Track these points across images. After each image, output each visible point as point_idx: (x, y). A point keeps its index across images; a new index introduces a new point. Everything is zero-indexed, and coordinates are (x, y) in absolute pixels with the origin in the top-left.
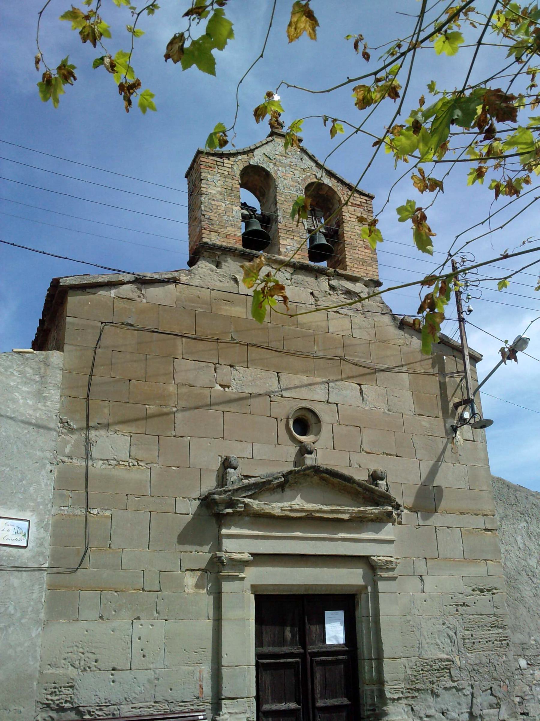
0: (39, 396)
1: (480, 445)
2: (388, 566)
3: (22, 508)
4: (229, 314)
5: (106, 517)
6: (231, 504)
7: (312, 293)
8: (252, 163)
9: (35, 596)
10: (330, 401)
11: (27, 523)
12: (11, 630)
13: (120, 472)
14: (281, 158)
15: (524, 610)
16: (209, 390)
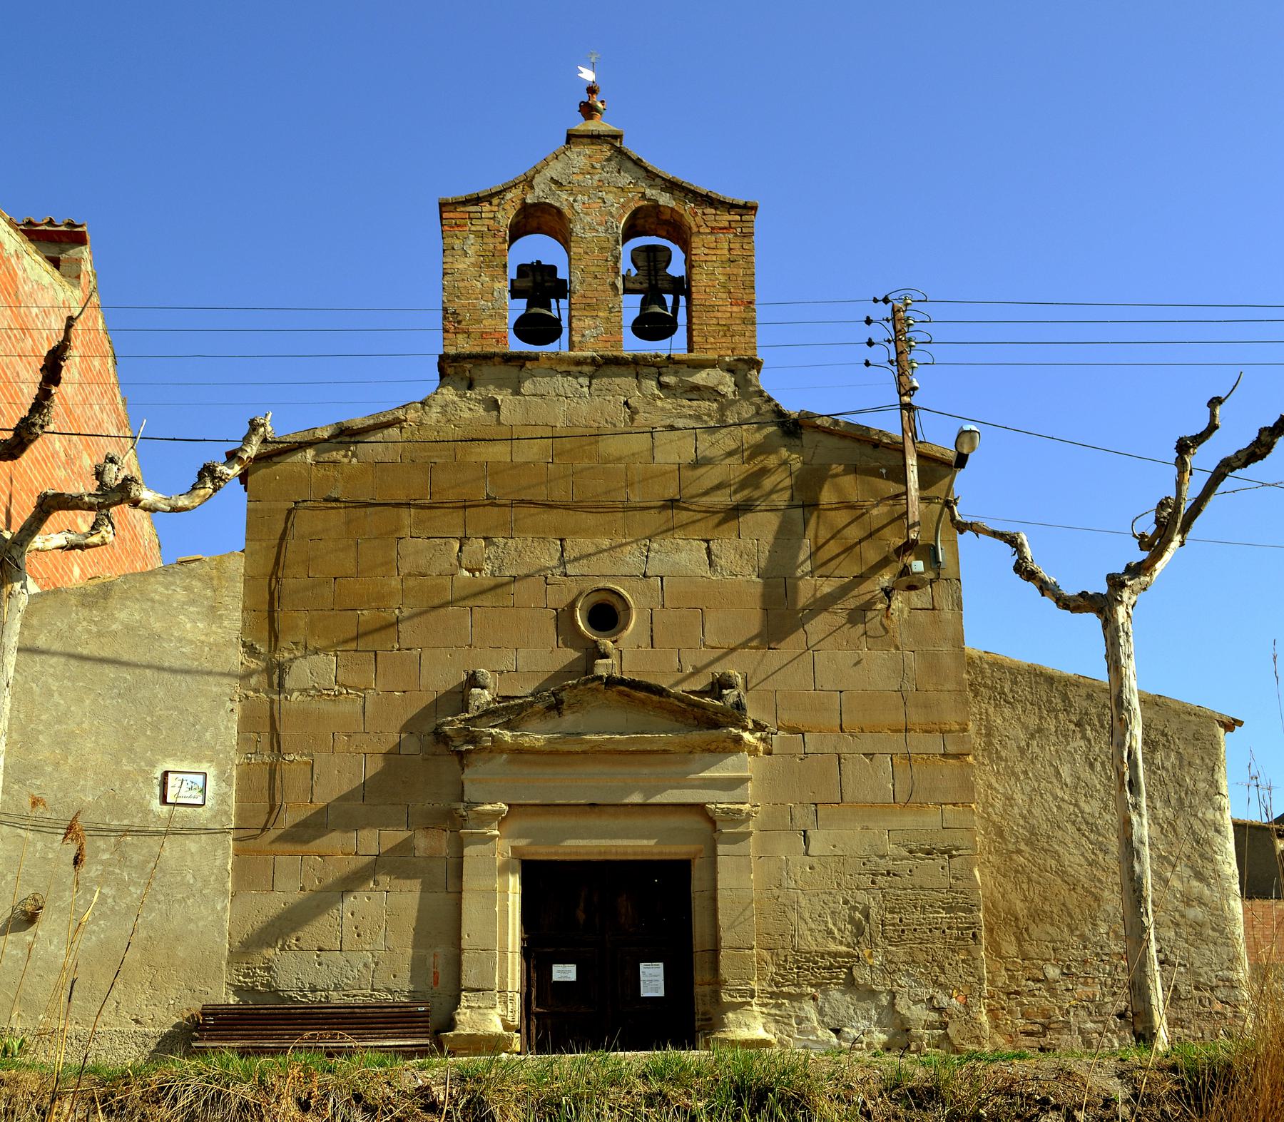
0: (213, 613)
1: (947, 614)
2: (735, 817)
3: (198, 759)
4: (482, 459)
5: (306, 763)
6: (474, 739)
7: (626, 403)
8: (529, 201)
9: (218, 863)
10: (649, 573)
11: (201, 777)
12: (190, 902)
13: (325, 706)
14: (581, 178)
15: (1065, 887)
16: (448, 579)
